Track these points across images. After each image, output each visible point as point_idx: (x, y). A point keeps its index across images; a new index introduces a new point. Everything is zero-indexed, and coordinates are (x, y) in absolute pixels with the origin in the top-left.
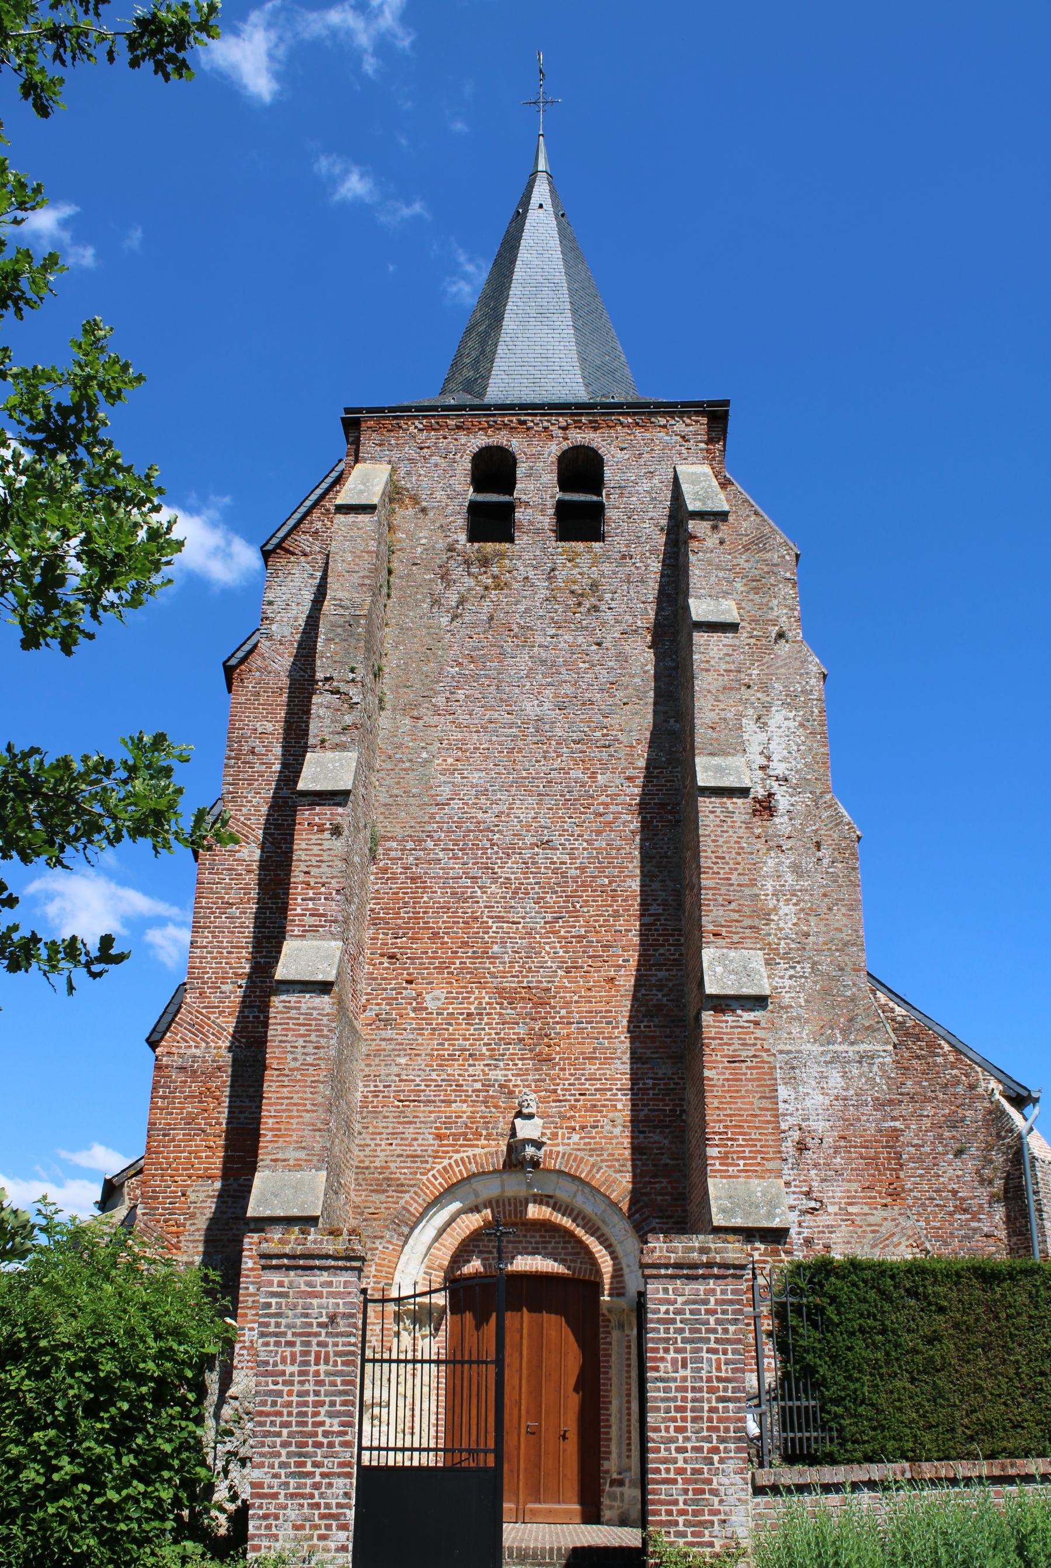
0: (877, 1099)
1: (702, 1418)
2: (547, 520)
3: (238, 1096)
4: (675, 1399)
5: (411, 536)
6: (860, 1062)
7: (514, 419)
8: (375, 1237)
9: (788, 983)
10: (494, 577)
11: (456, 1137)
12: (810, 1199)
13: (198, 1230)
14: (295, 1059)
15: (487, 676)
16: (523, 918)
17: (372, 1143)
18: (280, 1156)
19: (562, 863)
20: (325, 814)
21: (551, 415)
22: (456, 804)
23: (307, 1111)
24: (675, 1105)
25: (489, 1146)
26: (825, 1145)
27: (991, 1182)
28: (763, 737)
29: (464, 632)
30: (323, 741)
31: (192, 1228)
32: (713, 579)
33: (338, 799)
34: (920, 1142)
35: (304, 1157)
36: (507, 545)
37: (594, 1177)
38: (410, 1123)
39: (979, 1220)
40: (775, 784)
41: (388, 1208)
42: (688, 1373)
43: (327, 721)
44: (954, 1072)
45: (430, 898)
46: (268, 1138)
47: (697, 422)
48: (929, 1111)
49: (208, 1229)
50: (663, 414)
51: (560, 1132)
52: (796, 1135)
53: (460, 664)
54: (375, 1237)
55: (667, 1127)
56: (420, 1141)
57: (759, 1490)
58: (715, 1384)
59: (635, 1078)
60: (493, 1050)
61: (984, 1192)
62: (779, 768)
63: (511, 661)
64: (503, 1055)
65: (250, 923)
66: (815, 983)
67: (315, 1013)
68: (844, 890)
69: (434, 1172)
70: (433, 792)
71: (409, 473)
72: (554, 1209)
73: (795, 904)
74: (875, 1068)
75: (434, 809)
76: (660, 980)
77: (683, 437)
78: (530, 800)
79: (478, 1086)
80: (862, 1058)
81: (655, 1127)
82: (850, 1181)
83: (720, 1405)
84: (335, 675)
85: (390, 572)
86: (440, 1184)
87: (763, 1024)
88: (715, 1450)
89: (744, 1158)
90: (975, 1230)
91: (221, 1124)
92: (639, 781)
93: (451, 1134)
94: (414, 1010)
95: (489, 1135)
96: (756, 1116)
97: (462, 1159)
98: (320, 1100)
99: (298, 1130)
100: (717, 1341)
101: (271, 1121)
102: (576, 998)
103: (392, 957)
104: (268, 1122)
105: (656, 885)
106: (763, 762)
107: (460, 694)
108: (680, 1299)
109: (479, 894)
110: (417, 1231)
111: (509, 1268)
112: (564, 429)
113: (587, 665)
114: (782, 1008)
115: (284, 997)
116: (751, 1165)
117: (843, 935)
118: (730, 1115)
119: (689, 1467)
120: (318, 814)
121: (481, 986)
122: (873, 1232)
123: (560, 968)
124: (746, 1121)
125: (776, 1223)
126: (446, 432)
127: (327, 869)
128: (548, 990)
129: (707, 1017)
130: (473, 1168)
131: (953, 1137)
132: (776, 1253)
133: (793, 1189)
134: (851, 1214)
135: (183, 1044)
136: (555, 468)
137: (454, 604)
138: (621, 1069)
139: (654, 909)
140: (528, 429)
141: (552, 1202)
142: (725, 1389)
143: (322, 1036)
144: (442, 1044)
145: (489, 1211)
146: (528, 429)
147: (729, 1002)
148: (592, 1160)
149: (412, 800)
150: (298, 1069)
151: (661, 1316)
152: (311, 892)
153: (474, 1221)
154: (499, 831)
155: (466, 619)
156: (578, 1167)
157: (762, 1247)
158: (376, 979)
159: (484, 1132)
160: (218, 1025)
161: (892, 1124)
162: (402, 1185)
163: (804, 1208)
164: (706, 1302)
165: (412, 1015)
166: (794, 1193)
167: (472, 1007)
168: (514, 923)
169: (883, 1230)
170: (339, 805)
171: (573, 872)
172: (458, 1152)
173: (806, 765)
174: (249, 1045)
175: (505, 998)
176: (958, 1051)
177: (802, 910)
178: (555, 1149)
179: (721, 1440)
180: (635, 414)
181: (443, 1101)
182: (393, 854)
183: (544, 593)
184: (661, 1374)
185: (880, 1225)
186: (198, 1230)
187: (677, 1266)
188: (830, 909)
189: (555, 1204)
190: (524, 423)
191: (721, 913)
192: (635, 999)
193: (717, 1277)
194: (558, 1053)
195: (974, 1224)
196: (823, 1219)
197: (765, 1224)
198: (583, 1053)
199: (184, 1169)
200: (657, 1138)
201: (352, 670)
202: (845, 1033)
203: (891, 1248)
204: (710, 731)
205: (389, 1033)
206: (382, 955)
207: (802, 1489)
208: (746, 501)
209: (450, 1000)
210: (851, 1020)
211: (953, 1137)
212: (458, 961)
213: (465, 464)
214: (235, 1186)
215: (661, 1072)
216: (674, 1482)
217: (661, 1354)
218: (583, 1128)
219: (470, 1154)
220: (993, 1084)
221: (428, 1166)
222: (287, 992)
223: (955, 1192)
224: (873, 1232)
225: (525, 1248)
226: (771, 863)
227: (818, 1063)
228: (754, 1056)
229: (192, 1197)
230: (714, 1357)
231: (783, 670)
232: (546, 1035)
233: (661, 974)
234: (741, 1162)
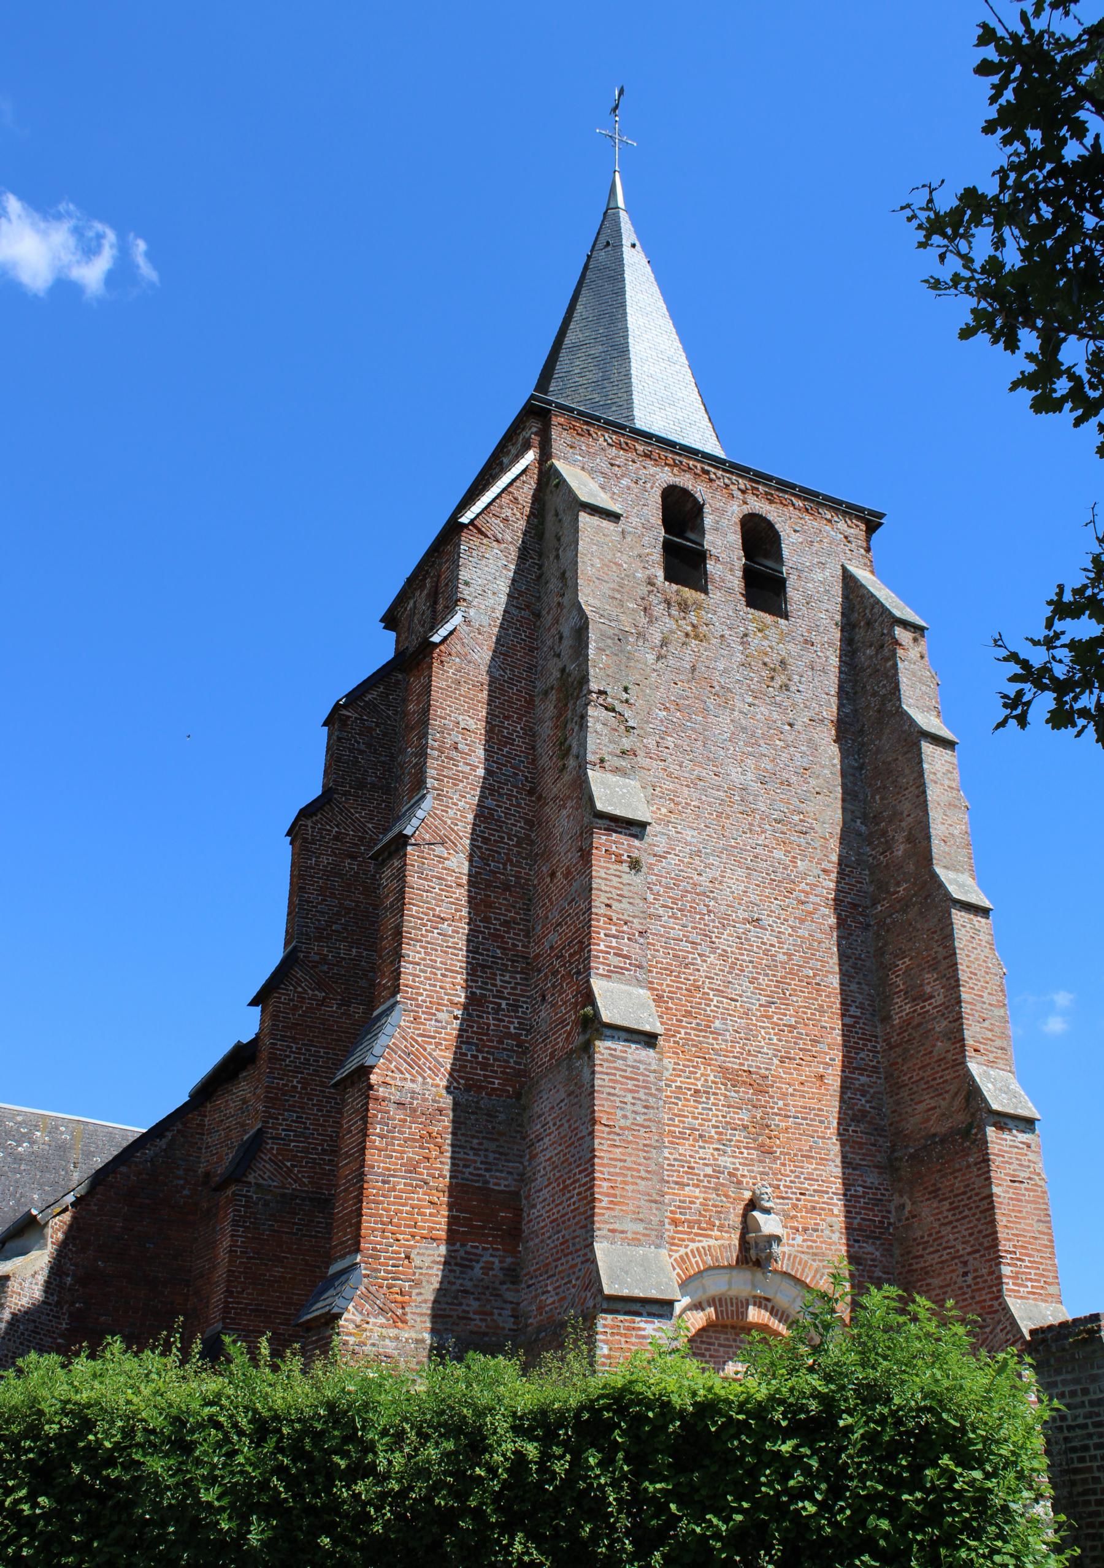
2: (736, 581)
3: (461, 1147)
7: (699, 465)
11: (691, 1224)
13: (425, 1301)
14: (625, 1117)
15: (693, 729)
16: (741, 996)
18: (617, 1226)
20: (620, 843)
22: (672, 859)
24: (883, 1217)
25: (722, 1238)
29: (669, 676)
30: (602, 761)
31: (419, 1299)
33: (635, 830)
36: (703, 596)
45: (654, 957)
46: (603, 1204)
47: (857, 526)
49: (435, 1302)
53: (666, 709)
55: (878, 1238)
59: (847, 1184)
60: (721, 1133)
63: (715, 720)
64: (730, 1140)
65: (462, 944)
67: (642, 1067)
72: (771, 1314)
76: (863, 1085)
77: (846, 537)
79: (709, 1170)
81: (868, 1237)
84: (609, 690)
89: (1031, 1280)
91: (444, 1177)
92: (834, 876)
95: (721, 1226)
99: (635, 1199)
101: (605, 1184)
102: (790, 1090)
104: (602, 1187)
105: (854, 987)
107: (670, 741)
109: (699, 961)
115: (608, 1044)
120: (615, 842)
121: (707, 1062)
123: (776, 1056)
126: (634, 455)
127: (628, 906)
129: (990, 1131)
130: (709, 1261)
135: (398, 1076)
136: (738, 528)
138: (834, 1169)
139: (853, 1010)
140: (711, 480)
141: (770, 1305)
143: (651, 1095)
145: (712, 1309)
148: (815, 1264)
152: (614, 928)
154: (714, 898)
156: (803, 1270)
159: (717, 1223)
160: (434, 1058)
170: (635, 836)
171: (782, 958)
172: (693, 1241)
174: (468, 1088)
180: (805, 499)
181: (677, 1183)
183: (740, 657)
186: (425, 1301)
189: (773, 1307)
190: (707, 473)
192: (842, 1100)
199: (407, 1226)
200: (870, 1249)
201: (626, 690)
204: (943, 844)
214: (462, 1253)
215: (869, 1180)
218: (805, 1230)
222: (612, 1038)
228: (1030, 1178)
229: (417, 1261)
232: (768, 1126)
233: (864, 1079)
234: (1029, 1284)
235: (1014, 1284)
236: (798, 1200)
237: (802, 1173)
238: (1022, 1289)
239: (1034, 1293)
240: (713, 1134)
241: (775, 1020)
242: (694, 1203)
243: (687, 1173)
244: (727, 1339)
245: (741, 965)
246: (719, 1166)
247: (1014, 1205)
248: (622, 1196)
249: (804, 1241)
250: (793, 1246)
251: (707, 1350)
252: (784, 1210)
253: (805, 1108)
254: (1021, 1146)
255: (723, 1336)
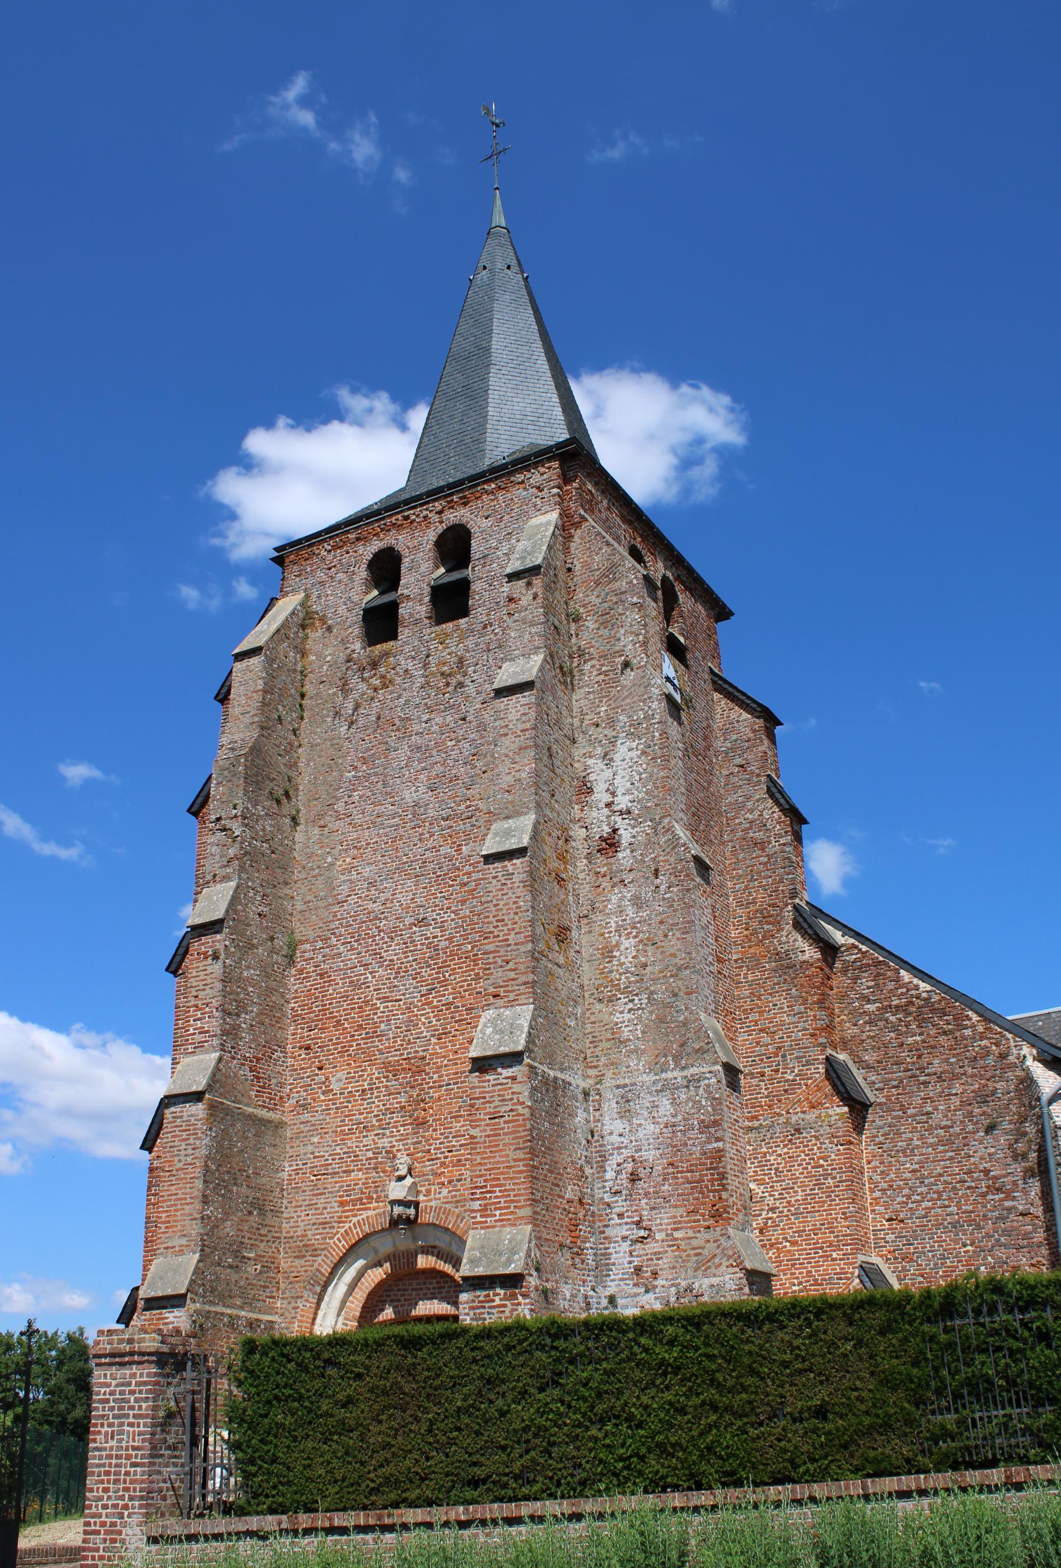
0: (703, 1121)
1: (119, 1480)
4: (104, 1465)
5: (320, 656)
6: (687, 1087)
7: (400, 517)
8: (297, 1297)
9: (627, 1016)
10: (383, 677)
11: (354, 1202)
12: (640, 1228)
14: (180, 1161)
15: (376, 774)
16: (404, 995)
17: (295, 1215)
18: (169, 1244)
19: (434, 937)
21: (428, 503)
23: (187, 1204)
26: (655, 1174)
27: (1024, 1156)
28: (608, 773)
30: (215, 876)
32: (527, 636)
33: (217, 927)
34: (949, 1123)
35: (185, 1243)
36: (392, 643)
37: (458, 1226)
38: (321, 1194)
39: (1014, 1198)
40: (618, 819)
41: (306, 1271)
42: (114, 1443)
43: (217, 857)
44: (983, 1043)
45: (334, 990)
48: (957, 1088)
50: (520, 471)
51: (433, 1188)
52: (629, 1167)
54: (297, 1297)
56: (329, 1210)
57: (154, 1540)
58: (130, 1452)
60: (381, 1120)
61: (1018, 1168)
62: (623, 802)
64: (389, 1123)
66: (651, 1012)
67: (192, 1119)
68: (678, 914)
69: (339, 1236)
70: (336, 892)
71: (319, 597)
72: (437, 1257)
73: (635, 937)
74: (701, 1091)
75: (336, 908)
77: (538, 488)
78: (409, 883)
79: (370, 1154)
80: (692, 1082)
82: (676, 1206)
83: (132, 1469)
85: (303, 696)
86: (343, 1246)
87: (519, 1079)
88: (126, 1507)
89: (500, 1208)
90: (1009, 1210)
93: (351, 1200)
94: (324, 1093)
95: (379, 1197)
96: (510, 1167)
97: (358, 1221)
98: (196, 1193)
99: (181, 1220)
100: (134, 1416)
102: (445, 1062)
103: (308, 1048)
106: (608, 798)
108: (114, 1383)
109: (370, 979)
110: (330, 1288)
111: (413, 1313)
112: (440, 512)
113: (453, 743)
114: (621, 1042)
115: (172, 1109)
116: (505, 1214)
117: (677, 960)
118: (489, 1169)
119: (108, 1520)
120: (203, 944)
122: (697, 1255)
123: (433, 1036)
124: (502, 1173)
125: (511, 1269)
128: (423, 1058)
131: (984, 1113)
132: (513, 1296)
133: (626, 1220)
134: (676, 1239)
137: (350, 712)
141: (436, 1251)
142: (136, 1456)
144: (343, 1121)
145: (388, 1264)
146: (411, 522)
147: (491, 1062)
149: (321, 904)
150: (182, 1169)
151: (101, 1397)
153: (377, 1275)
155: (360, 724)
157: (502, 1292)
158: (296, 1070)
159: (375, 1196)
161: (715, 1145)
162: (316, 1250)
163: (634, 1237)
164: (129, 1384)
165: (323, 1098)
166: (626, 1223)
167: (366, 1084)
168: (397, 1001)
169: (705, 1252)
170: (217, 932)
171: (443, 944)
172: (355, 1216)
173: (647, 793)
175: (390, 1071)
176: (987, 1020)
177: (641, 941)
178: (429, 1204)
179: (131, 1498)
180: (496, 478)
181: (344, 1172)
182: (307, 955)
184: (98, 1445)
185: (703, 1248)
187: (112, 1355)
188: (666, 936)
189: (439, 1253)
190: (407, 518)
191: (500, 974)
193: (139, 1363)
194: (431, 1115)
195: (1007, 1204)
196: (652, 1247)
197: (502, 1271)
198: (451, 1113)
202: (677, 1058)
203: (713, 1270)
204: (506, 795)
205: (306, 1116)
206: (300, 1048)
207: (191, 1538)
208: (599, 534)
209: (349, 1079)
210: (682, 1045)
211: (984, 1113)
212: (354, 1044)
213: (362, 573)
216: (98, 1532)
217: (99, 1428)
218: (450, 1182)
219: (364, 1216)
220: (1026, 1050)
221: (334, 1231)
222: (175, 1104)
223: (986, 1172)
224: (697, 1255)
225: (425, 1294)
226: (614, 899)
227: (650, 1093)
228: (511, 1110)
230: (132, 1430)
231: (628, 701)
232: (422, 1101)
234: (498, 1213)
235: (481, 1216)
236: (446, 1157)
237: (451, 1133)
238: (488, 1220)
239: (502, 1220)
240: (374, 1122)
241: (435, 1003)
242: (357, 1184)
243: (353, 1161)
244: (419, 1284)
245: (406, 967)
246: (378, 1148)
247: (490, 1141)
248: (174, 1221)
249: (449, 1192)
250: (439, 1199)
251: (402, 1295)
252: (433, 1170)
253: (457, 1073)
254: (505, 1081)
255: (415, 1282)
